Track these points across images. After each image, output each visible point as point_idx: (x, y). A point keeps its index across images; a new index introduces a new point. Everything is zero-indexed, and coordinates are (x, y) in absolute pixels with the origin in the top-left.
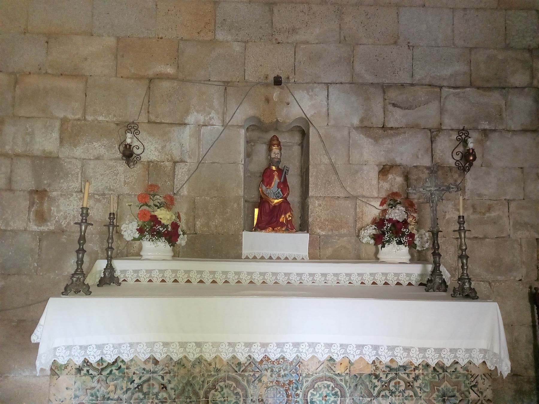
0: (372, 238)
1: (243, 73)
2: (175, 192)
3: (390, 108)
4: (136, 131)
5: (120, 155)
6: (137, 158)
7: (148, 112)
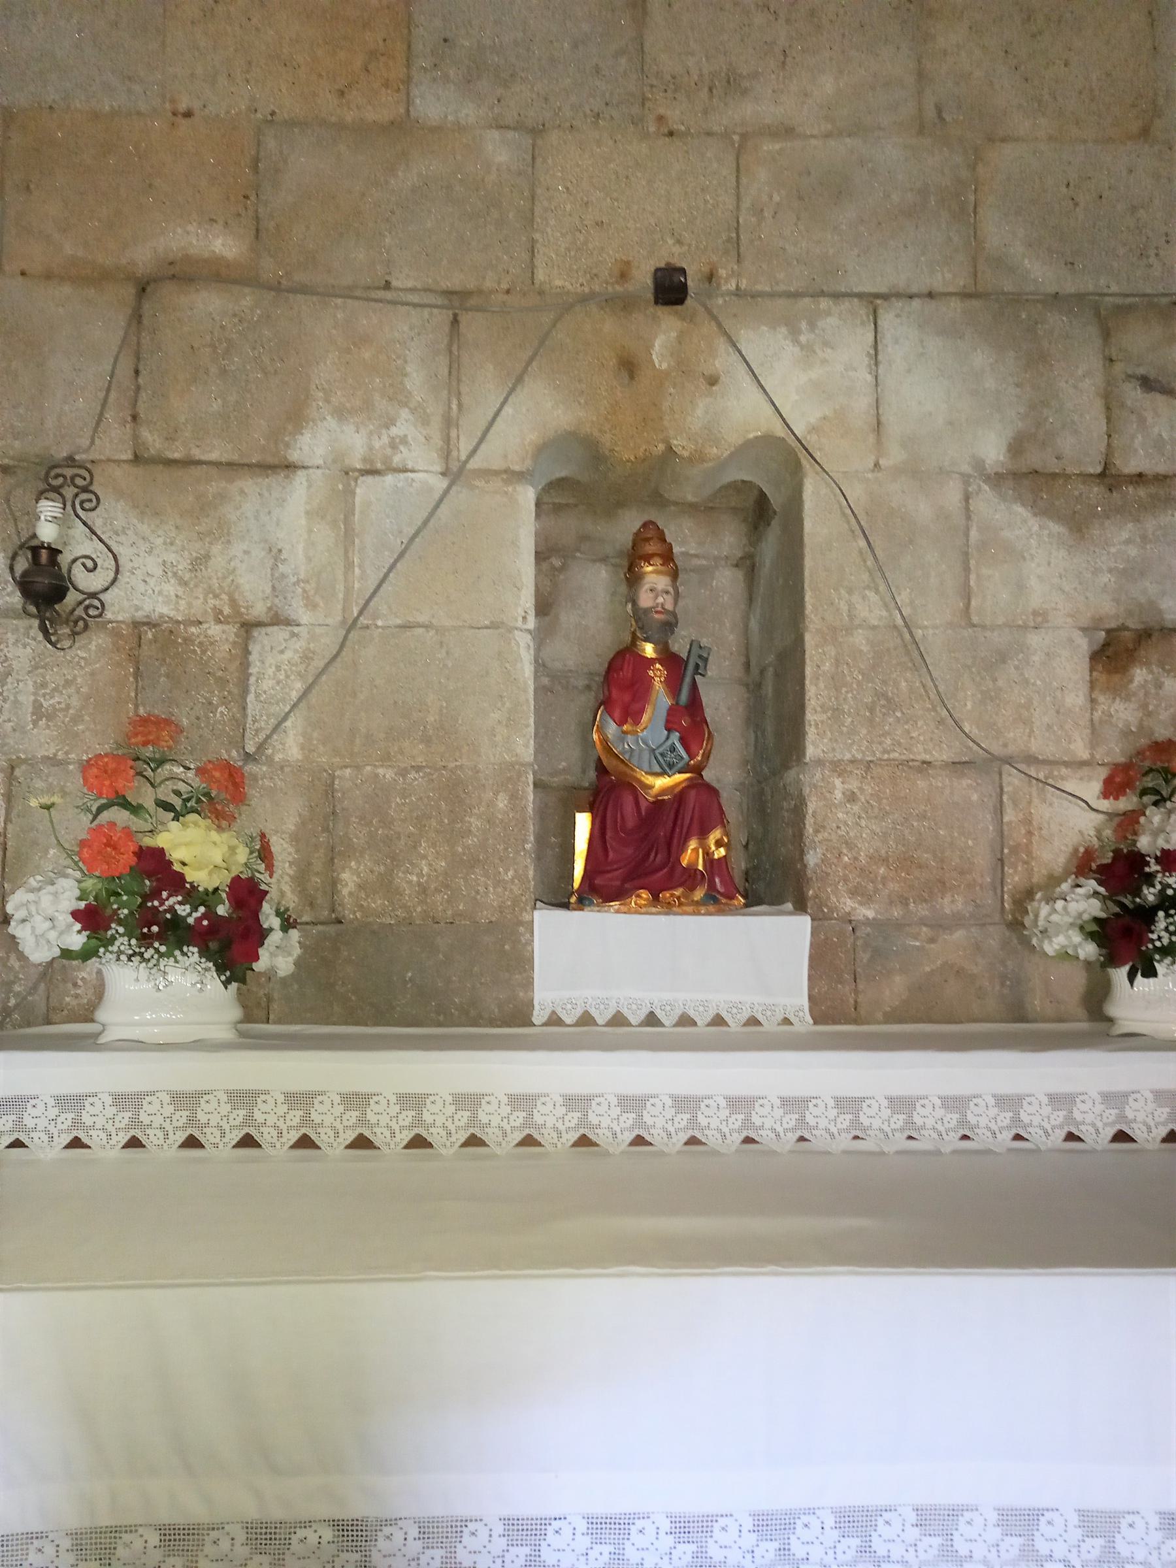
0: (1092, 936)
1: (525, 256)
2: (251, 749)
3: (1133, 394)
4: (84, 496)
5: (16, 599)
6: (87, 608)
7: (135, 417)
